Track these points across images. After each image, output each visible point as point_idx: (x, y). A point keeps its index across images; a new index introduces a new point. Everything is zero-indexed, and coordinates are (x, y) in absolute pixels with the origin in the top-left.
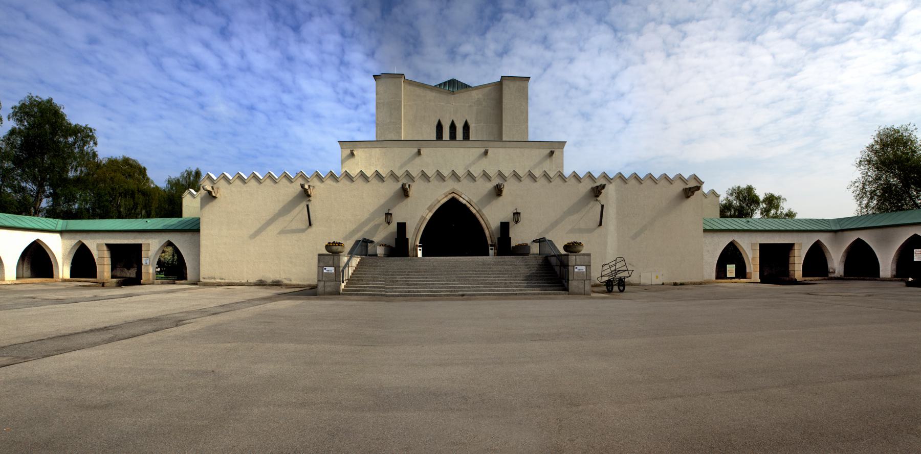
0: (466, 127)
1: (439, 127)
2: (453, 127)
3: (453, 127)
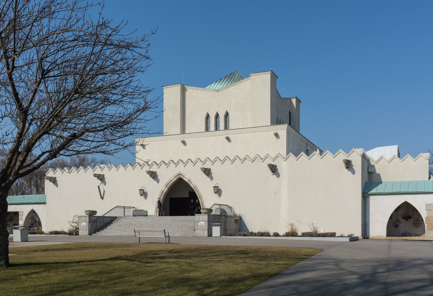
0: (227, 115)
1: (208, 117)
2: (217, 116)
3: (217, 116)
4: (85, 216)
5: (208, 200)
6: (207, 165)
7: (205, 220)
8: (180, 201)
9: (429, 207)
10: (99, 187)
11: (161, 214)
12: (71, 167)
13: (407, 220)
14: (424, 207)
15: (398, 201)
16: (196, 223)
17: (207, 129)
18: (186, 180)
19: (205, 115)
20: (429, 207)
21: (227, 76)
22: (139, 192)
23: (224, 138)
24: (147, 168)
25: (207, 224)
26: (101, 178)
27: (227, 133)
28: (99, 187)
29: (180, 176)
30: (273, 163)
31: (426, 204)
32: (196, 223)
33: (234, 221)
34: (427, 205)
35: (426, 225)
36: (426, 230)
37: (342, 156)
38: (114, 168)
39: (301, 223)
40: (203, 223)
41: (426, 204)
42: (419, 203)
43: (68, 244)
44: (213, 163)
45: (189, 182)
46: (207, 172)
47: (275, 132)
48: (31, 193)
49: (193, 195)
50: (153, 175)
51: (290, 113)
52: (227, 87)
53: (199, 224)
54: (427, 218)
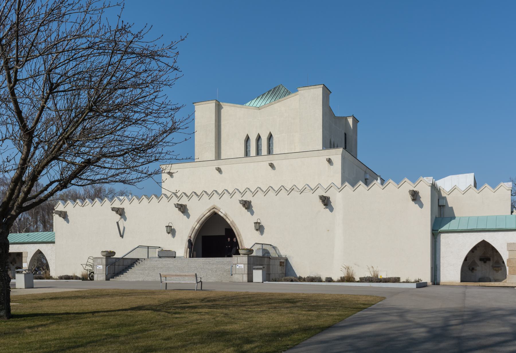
0: (270, 137)
1: (247, 139)
2: (259, 138)
3: (259, 138)
4: (102, 258)
5: (248, 238)
6: (247, 197)
7: (244, 263)
8: (215, 239)
9: (511, 247)
10: (117, 223)
11: (192, 255)
12: (85, 199)
13: (485, 262)
14: (505, 247)
15: (475, 239)
16: (234, 266)
17: (247, 154)
18: (222, 215)
19: (244, 137)
20: (511, 247)
21: (271, 90)
22: (165, 229)
23: (266, 164)
24: (175, 200)
25: (247, 267)
26: (120, 212)
27: (270, 159)
28: (117, 223)
29: (214, 210)
30: (325, 195)
31: (508, 244)
32: (234, 266)
33: (279, 264)
34: (509, 245)
35: (507, 268)
36: (508, 274)
37: (408, 186)
38: (136, 201)
39: (359, 266)
40: (242, 266)
41: (508, 244)
42: (499, 242)
43: (81, 291)
44: (254, 194)
45: (225, 217)
46: (247, 205)
47: (328, 157)
48: (37, 230)
49: (230, 233)
50: (183, 209)
51: (345, 134)
52: (270, 104)
53: (237, 267)
54: (508, 260)
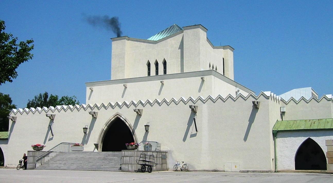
0: (165, 63)
1: (149, 65)
2: (157, 64)
3: (157, 64)
16: (122, 158)
17: (149, 74)
19: (146, 62)
27: (162, 78)
35: (327, 159)
36: (327, 163)
45: (125, 121)
51: (223, 59)
